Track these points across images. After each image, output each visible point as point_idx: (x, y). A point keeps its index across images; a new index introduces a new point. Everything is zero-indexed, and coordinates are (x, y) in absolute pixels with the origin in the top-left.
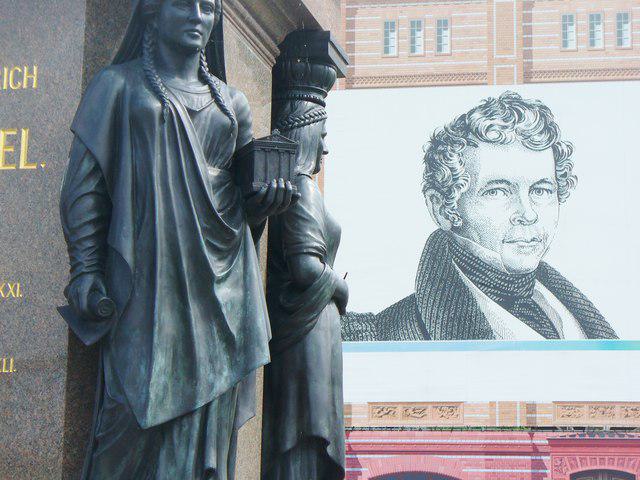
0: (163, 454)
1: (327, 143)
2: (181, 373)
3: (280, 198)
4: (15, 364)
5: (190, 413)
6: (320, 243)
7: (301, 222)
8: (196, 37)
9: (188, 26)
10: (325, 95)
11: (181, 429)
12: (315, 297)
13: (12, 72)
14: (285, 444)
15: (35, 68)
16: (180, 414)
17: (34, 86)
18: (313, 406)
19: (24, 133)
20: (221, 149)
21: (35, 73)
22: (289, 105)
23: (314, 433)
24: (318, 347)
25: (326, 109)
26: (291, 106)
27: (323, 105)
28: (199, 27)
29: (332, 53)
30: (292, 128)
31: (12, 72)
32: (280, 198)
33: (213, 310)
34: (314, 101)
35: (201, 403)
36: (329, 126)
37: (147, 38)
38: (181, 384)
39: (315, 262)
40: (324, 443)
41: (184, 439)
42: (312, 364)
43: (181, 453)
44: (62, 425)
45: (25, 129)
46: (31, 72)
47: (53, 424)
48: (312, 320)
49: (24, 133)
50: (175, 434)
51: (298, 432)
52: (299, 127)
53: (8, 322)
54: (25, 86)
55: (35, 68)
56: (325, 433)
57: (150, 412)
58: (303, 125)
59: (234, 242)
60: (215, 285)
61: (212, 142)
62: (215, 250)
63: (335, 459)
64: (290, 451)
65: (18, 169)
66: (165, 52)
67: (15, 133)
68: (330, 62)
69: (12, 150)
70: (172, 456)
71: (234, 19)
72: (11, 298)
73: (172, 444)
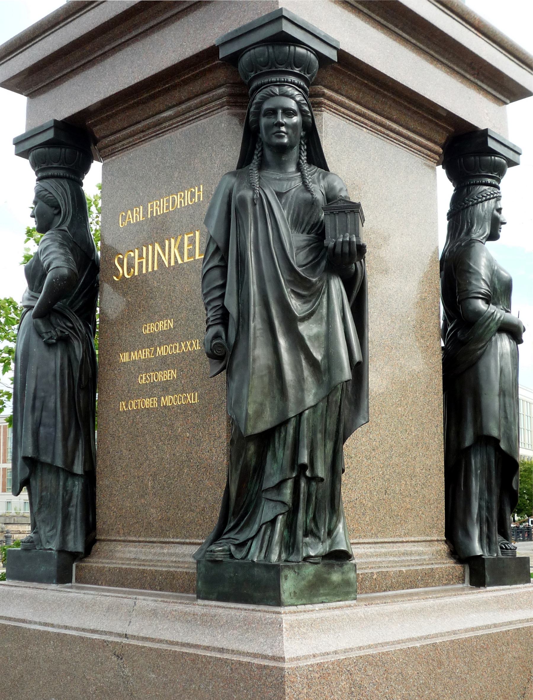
0: (270, 454)
1: (504, 216)
2: (276, 391)
3: (347, 249)
4: (198, 396)
5: (285, 422)
6: (169, 263)
7: (468, 275)
8: (282, 137)
9: (275, 129)
10: (499, 181)
11: (280, 435)
12: (481, 331)
13: (189, 193)
14: (464, 443)
15: (201, 186)
16: (277, 423)
17: (201, 199)
18: (484, 414)
19: (197, 233)
20: (306, 219)
21: (201, 190)
22: (466, 190)
23: (485, 433)
24: (488, 369)
25: (500, 191)
26: (467, 191)
27: (499, 188)
28: (283, 129)
29: (492, 144)
30: (468, 207)
31: (189, 193)
32: (347, 249)
33: (298, 343)
34: (491, 185)
35: (291, 414)
36: (502, 204)
37: (257, 147)
38: (276, 402)
39: (481, 305)
40: (496, 441)
41: (282, 442)
42: (483, 383)
43: (280, 454)
44: (225, 437)
45: (198, 231)
46: (199, 190)
47: (220, 437)
48: (483, 346)
49: (197, 233)
50: (277, 440)
51: (474, 433)
52: (472, 205)
53: (194, 367)
54: (196, 201)
55: (201, 186)
56: (495, 433)
57: (250, 423)
58: (477, 204)
59: (314, 289)
60: (299, 323)
61: (298, 215)
62: (299, 296)
63: (508, 452)
64: (469, 448)
65: (195, 260)
66: (268, 153)
67: (192, 235)
68: (495, 153)
69: (191, 247)
70: (274, 455)
71: (371, 127)
72: (194, 351)
73: (274, 447)
